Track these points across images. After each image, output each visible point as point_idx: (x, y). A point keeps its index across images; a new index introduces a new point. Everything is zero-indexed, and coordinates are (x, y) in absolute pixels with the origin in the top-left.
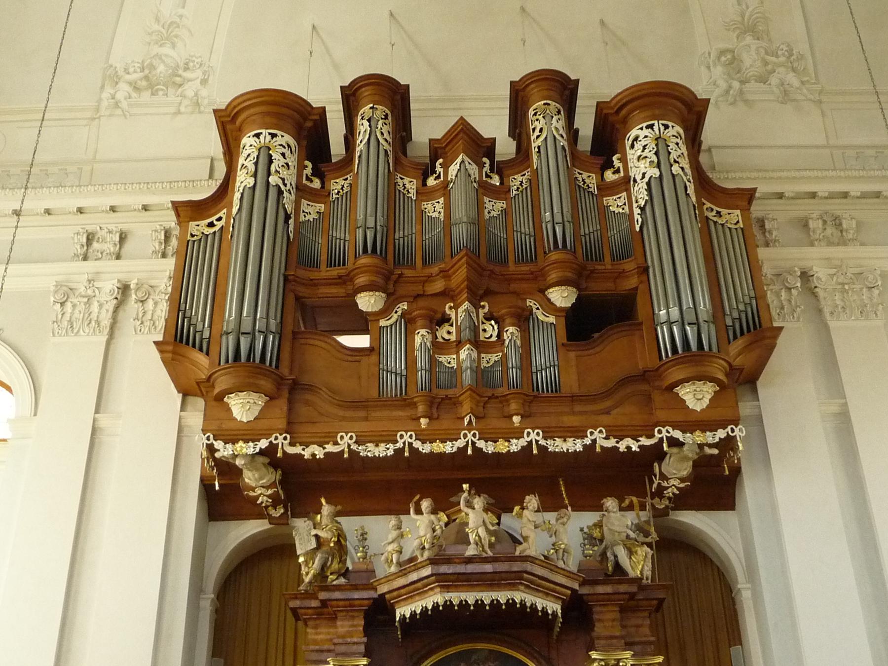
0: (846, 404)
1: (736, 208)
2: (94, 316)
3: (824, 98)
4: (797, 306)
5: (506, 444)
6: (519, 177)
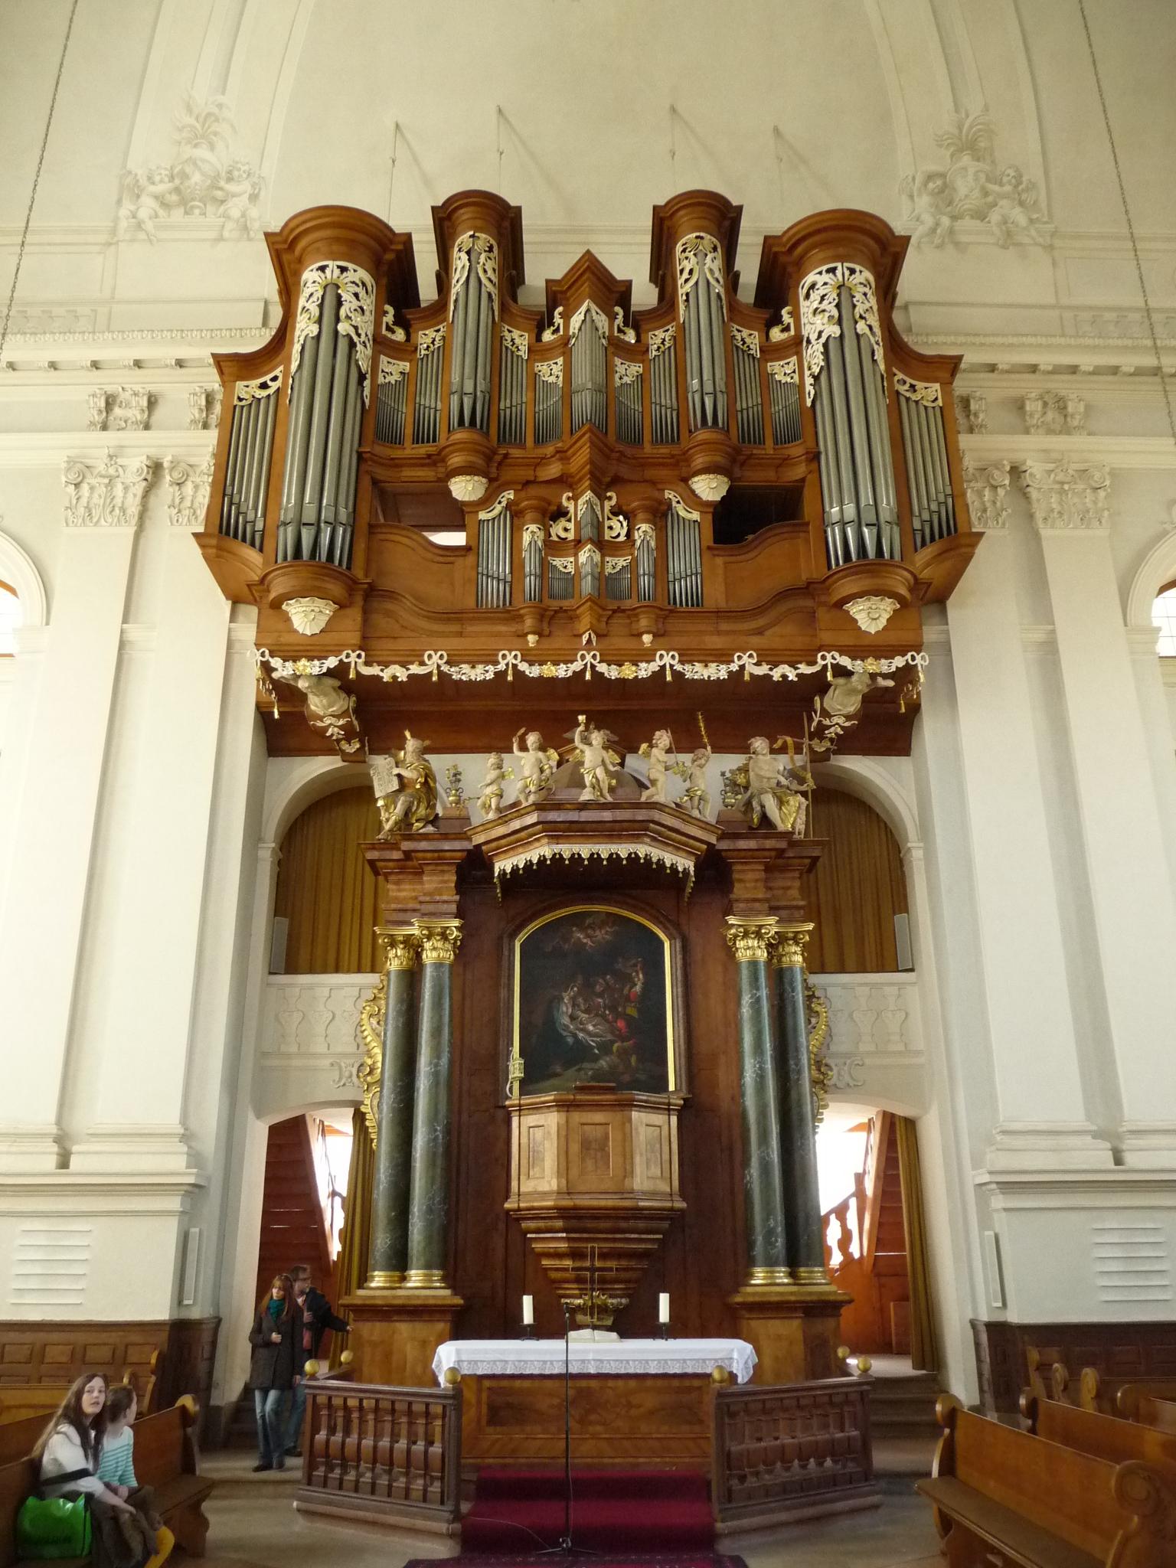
2: (118, 501)
5: (634, 668)
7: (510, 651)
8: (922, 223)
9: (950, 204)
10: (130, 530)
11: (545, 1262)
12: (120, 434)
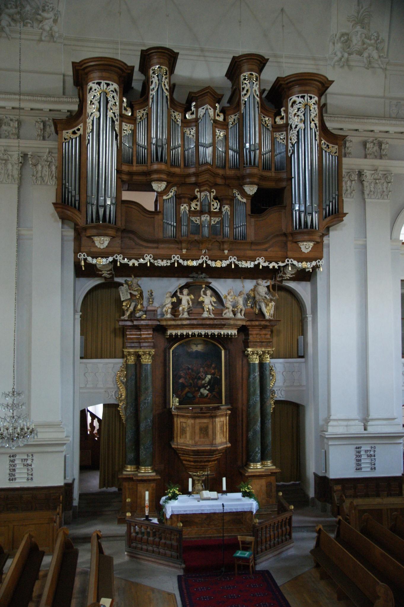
0: (366, 241)
1: (336, 144)
2: (10, 172)
3: (388, 67)
4: (354, 190)
6: (233, 116)
7: (176, 255)
8: (337, 56)
9: (349, 48)
10: (16, 186)
11: (184, 462)
12: (7, 140)
